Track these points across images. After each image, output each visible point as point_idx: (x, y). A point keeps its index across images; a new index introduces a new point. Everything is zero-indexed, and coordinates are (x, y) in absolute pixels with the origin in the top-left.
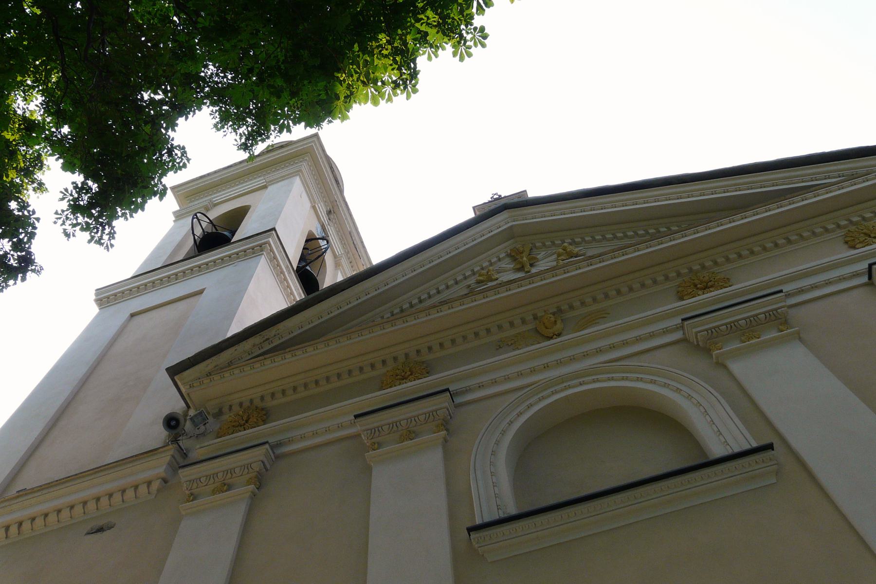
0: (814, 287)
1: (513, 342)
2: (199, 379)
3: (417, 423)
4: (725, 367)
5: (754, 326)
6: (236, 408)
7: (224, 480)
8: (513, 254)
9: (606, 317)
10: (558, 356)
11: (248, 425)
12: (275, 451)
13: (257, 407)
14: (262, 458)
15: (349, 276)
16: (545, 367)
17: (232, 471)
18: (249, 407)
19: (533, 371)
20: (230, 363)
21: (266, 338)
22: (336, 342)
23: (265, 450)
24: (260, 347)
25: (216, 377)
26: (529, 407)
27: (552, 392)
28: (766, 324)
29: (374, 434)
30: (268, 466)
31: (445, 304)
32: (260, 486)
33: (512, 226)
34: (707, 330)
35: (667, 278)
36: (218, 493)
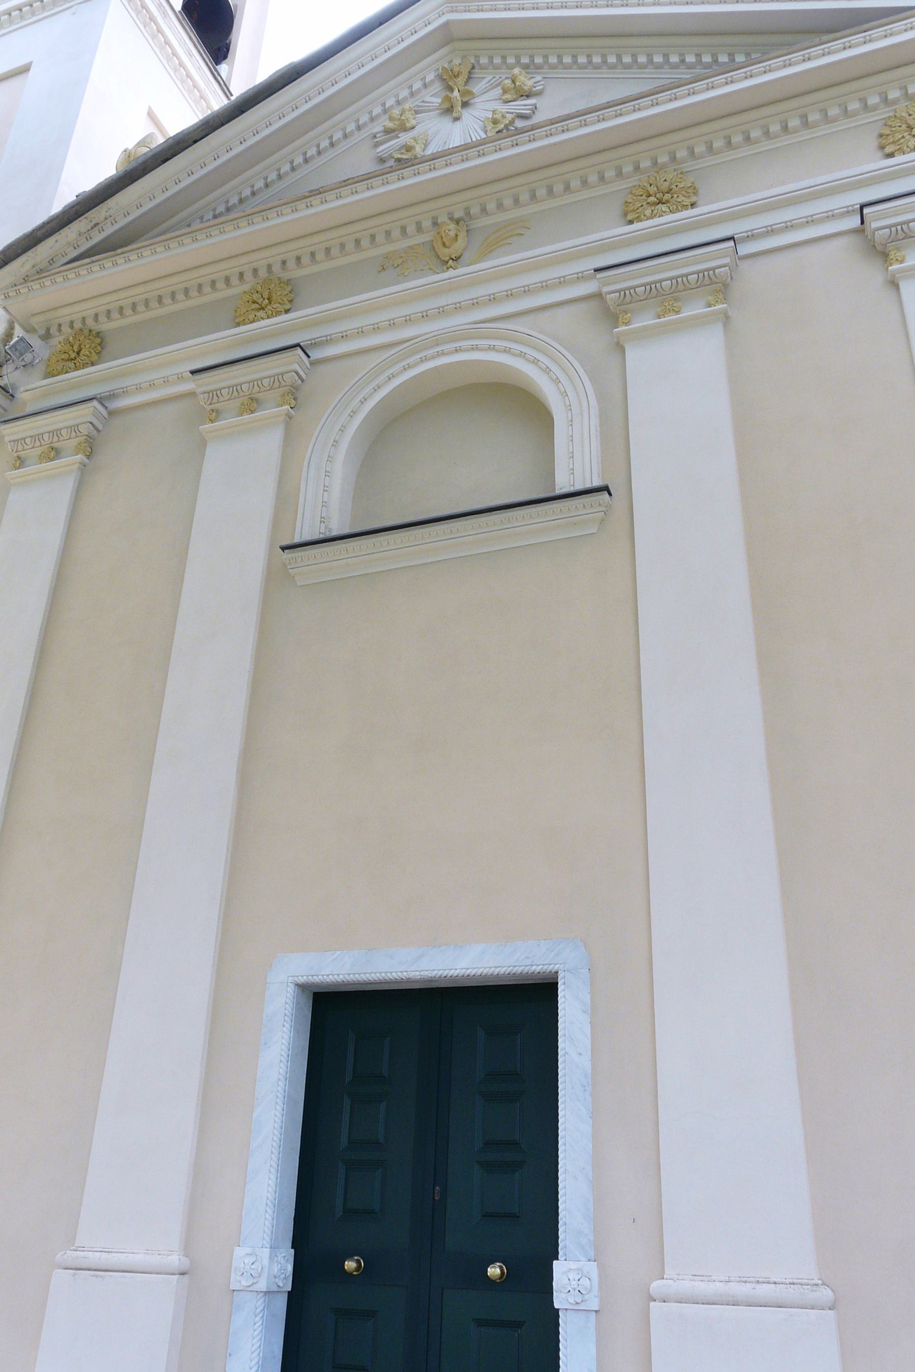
0: (789, 227)
1: (400, 261)
2: (15, 286)
3: (260, 388)
4: (622, 350)
5: (680, 291)
6: (66, 329)
7: (51, 443)
8: (444, 77)
9: (522, 234)
10: (442, 301)
11: (80, 361)
12: (107, 405)
13: (90, 331)
14: (91, 418)
15: (201, 118)
16: (423, 316)
17: (56, 432)
18: (81, 330)
19: (408, 321)
20: (51, 261)
21: (94, 222)
22: (179, 244)
23: (91, 409)
24: (88, 238)
25: (36, 286)
26: (389, 379)
27: (421, 358)
28: (698, 289)
29: (212, 399)
30: (100, 427)
31: (318, 194)
32: (91, 453)
33: (447, 24)
34: (619, 291)
35: (620, 174)
36: (44, 461)
